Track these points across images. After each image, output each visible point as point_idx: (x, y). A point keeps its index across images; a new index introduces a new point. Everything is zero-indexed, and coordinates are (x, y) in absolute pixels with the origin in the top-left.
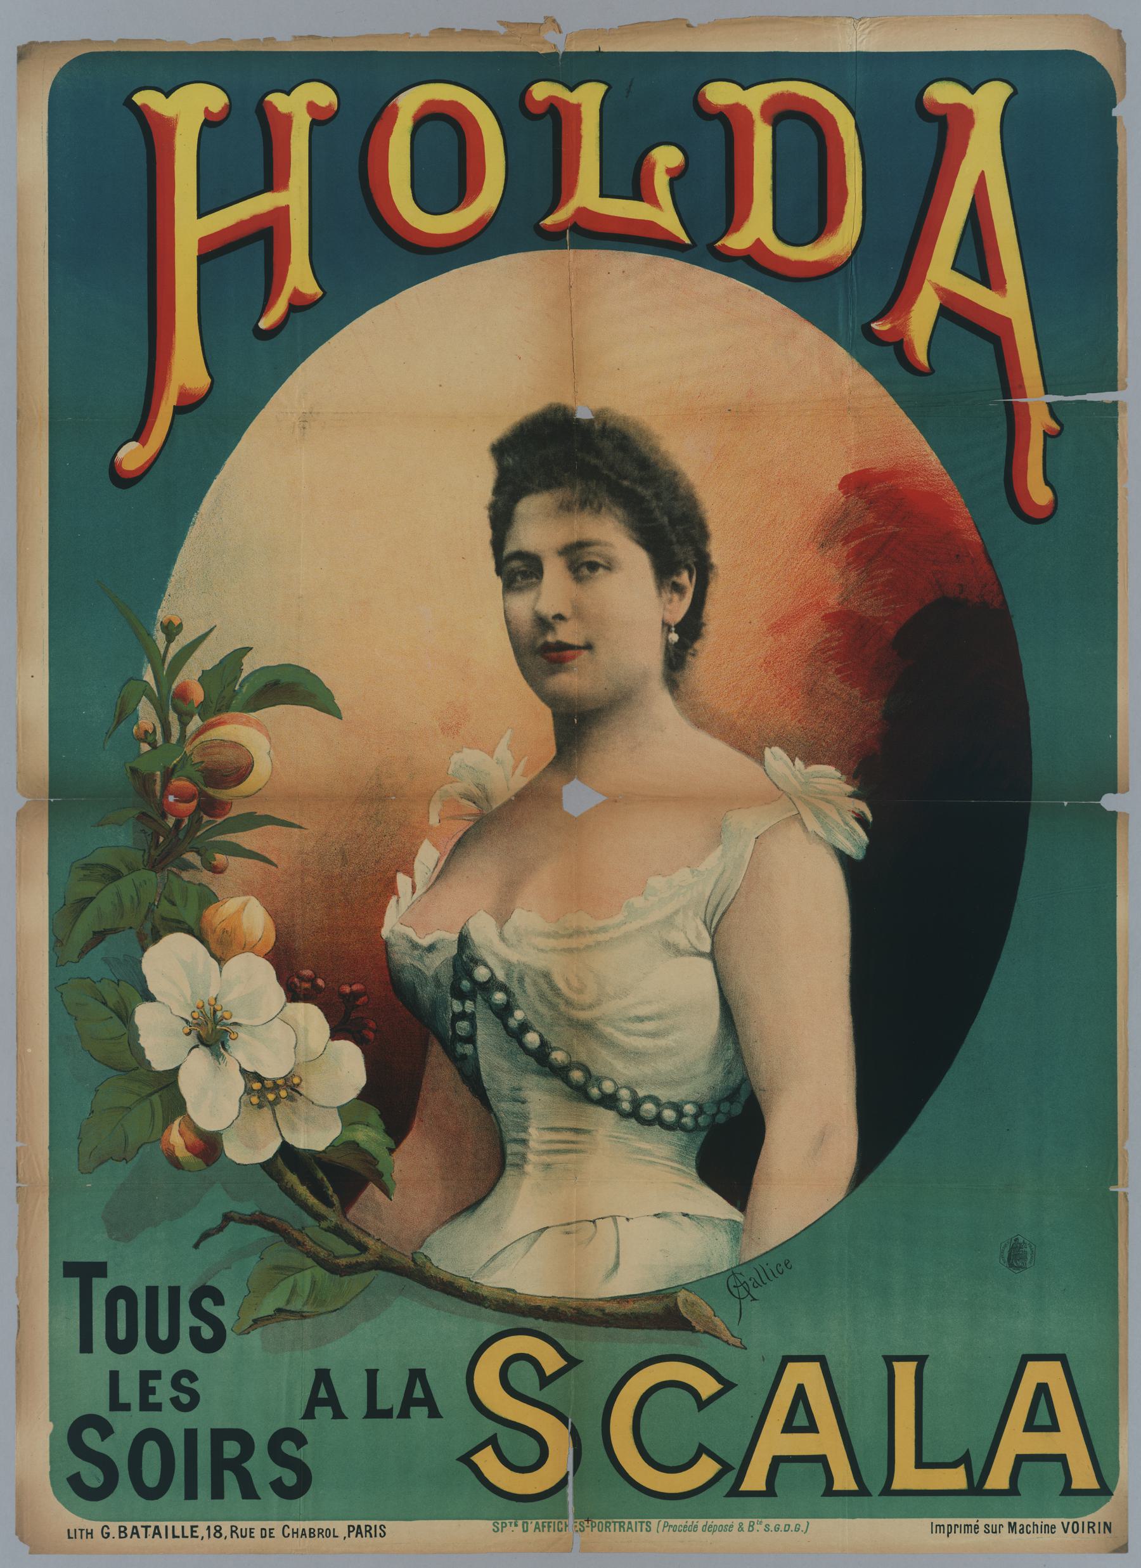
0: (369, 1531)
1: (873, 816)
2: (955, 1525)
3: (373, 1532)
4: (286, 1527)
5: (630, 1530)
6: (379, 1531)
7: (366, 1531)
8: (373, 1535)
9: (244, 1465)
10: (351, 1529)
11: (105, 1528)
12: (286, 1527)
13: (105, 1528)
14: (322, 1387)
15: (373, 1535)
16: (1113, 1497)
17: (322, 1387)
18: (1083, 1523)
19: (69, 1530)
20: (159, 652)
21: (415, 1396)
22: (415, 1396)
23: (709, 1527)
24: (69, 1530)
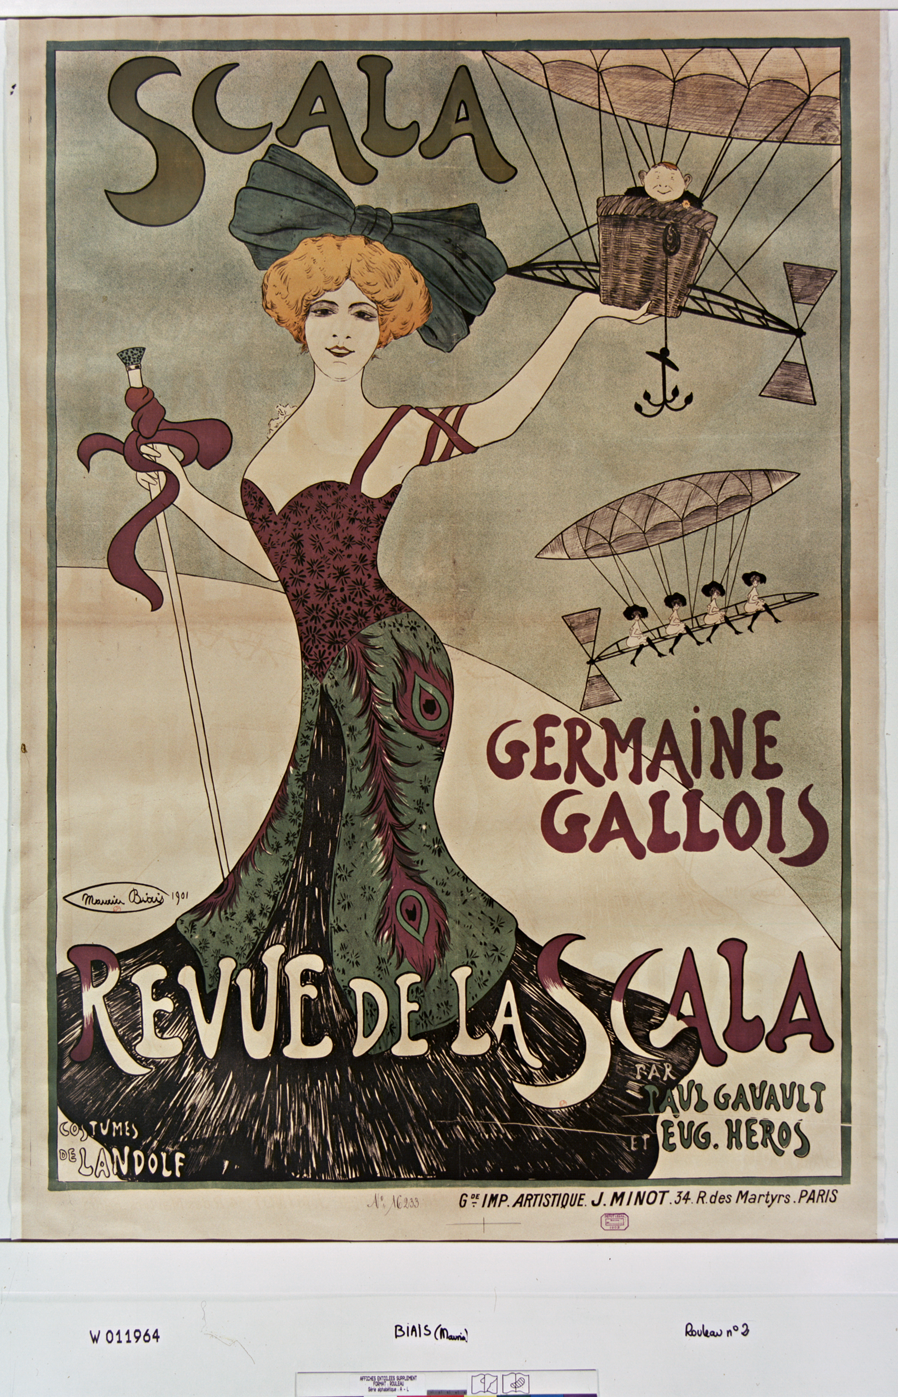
0: (822, 1196)
1: (735, 746)
2: (760, 1196)
3: (824, 1197)
4: (596, 1202)
5: (95, 1333)
6: (831, 1195)
7: (819, 1195)
8: (824, 1200)
9: (546, 736)
10: (804, 1193)
11: (464, 1196)
12: (596, 1202)
13: (464, 1196)
14: (800, 1005)
15: (824, 1200)
16: (675, 1018)
17: (800, 1005)
18: (631, 1193)
19: (661, 1203)
20: (492, 51)
21: (665, 753)
22: (665, 753)
23: (720, 1198)
24: (661, 1203)
